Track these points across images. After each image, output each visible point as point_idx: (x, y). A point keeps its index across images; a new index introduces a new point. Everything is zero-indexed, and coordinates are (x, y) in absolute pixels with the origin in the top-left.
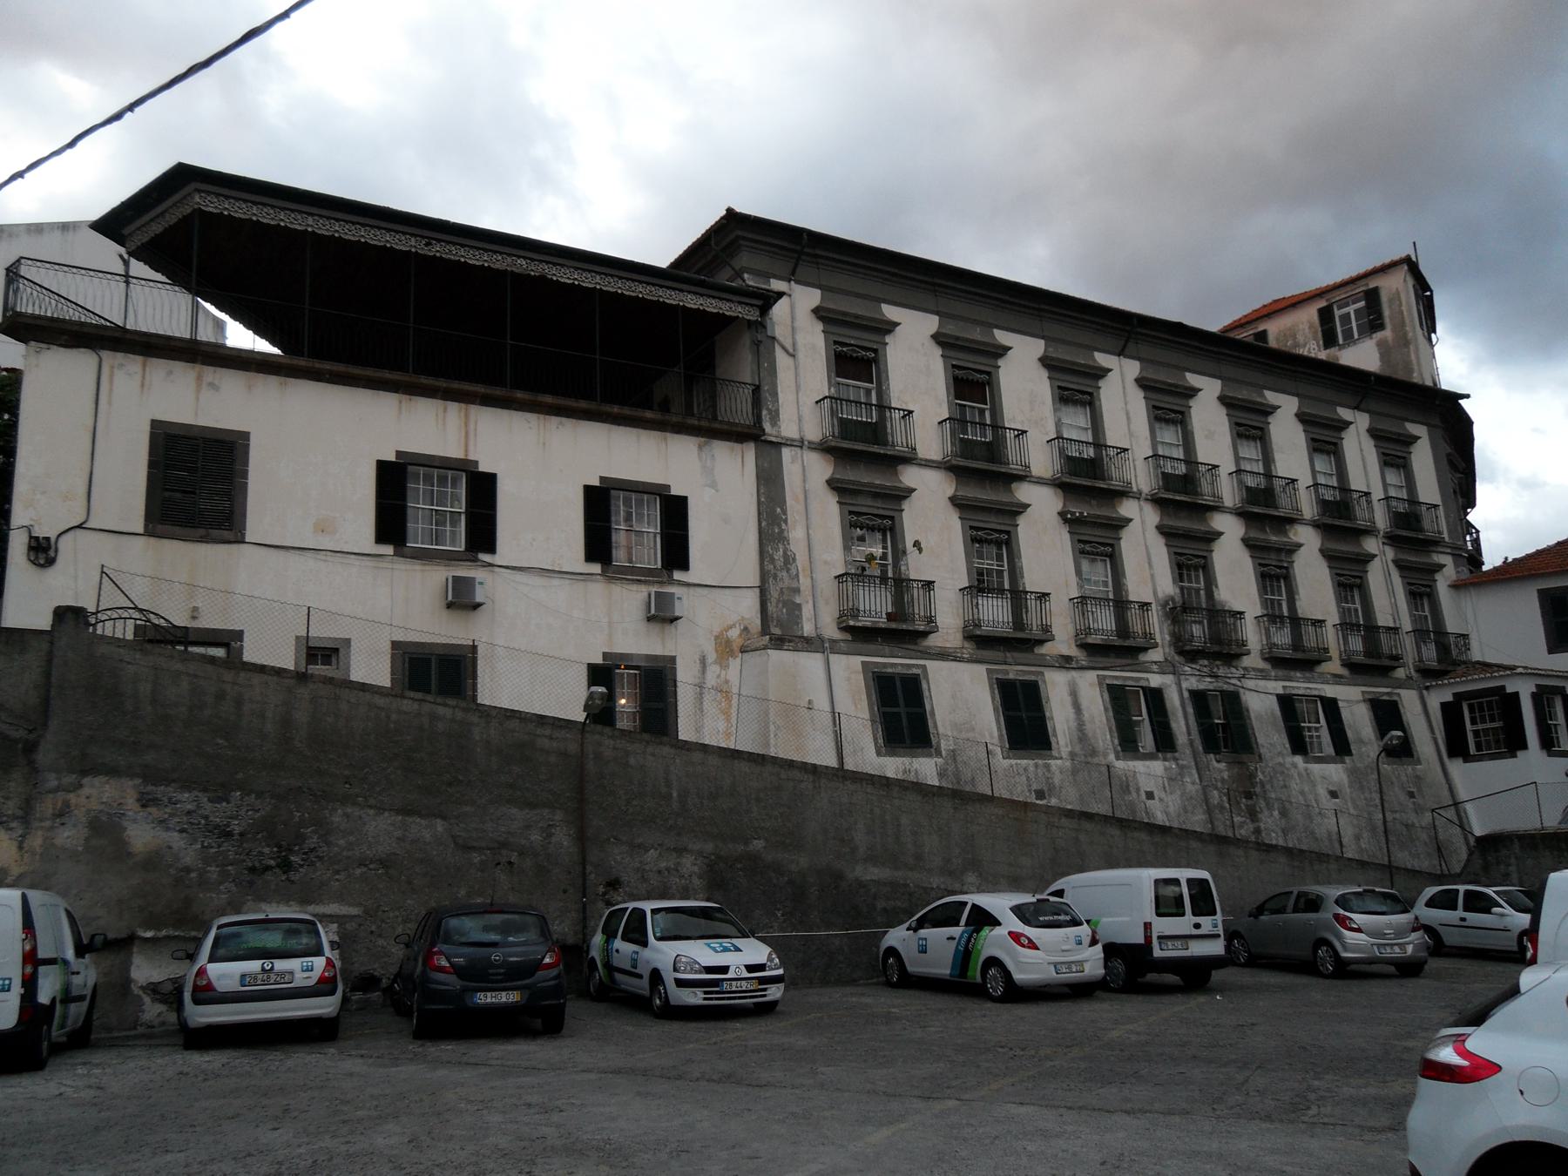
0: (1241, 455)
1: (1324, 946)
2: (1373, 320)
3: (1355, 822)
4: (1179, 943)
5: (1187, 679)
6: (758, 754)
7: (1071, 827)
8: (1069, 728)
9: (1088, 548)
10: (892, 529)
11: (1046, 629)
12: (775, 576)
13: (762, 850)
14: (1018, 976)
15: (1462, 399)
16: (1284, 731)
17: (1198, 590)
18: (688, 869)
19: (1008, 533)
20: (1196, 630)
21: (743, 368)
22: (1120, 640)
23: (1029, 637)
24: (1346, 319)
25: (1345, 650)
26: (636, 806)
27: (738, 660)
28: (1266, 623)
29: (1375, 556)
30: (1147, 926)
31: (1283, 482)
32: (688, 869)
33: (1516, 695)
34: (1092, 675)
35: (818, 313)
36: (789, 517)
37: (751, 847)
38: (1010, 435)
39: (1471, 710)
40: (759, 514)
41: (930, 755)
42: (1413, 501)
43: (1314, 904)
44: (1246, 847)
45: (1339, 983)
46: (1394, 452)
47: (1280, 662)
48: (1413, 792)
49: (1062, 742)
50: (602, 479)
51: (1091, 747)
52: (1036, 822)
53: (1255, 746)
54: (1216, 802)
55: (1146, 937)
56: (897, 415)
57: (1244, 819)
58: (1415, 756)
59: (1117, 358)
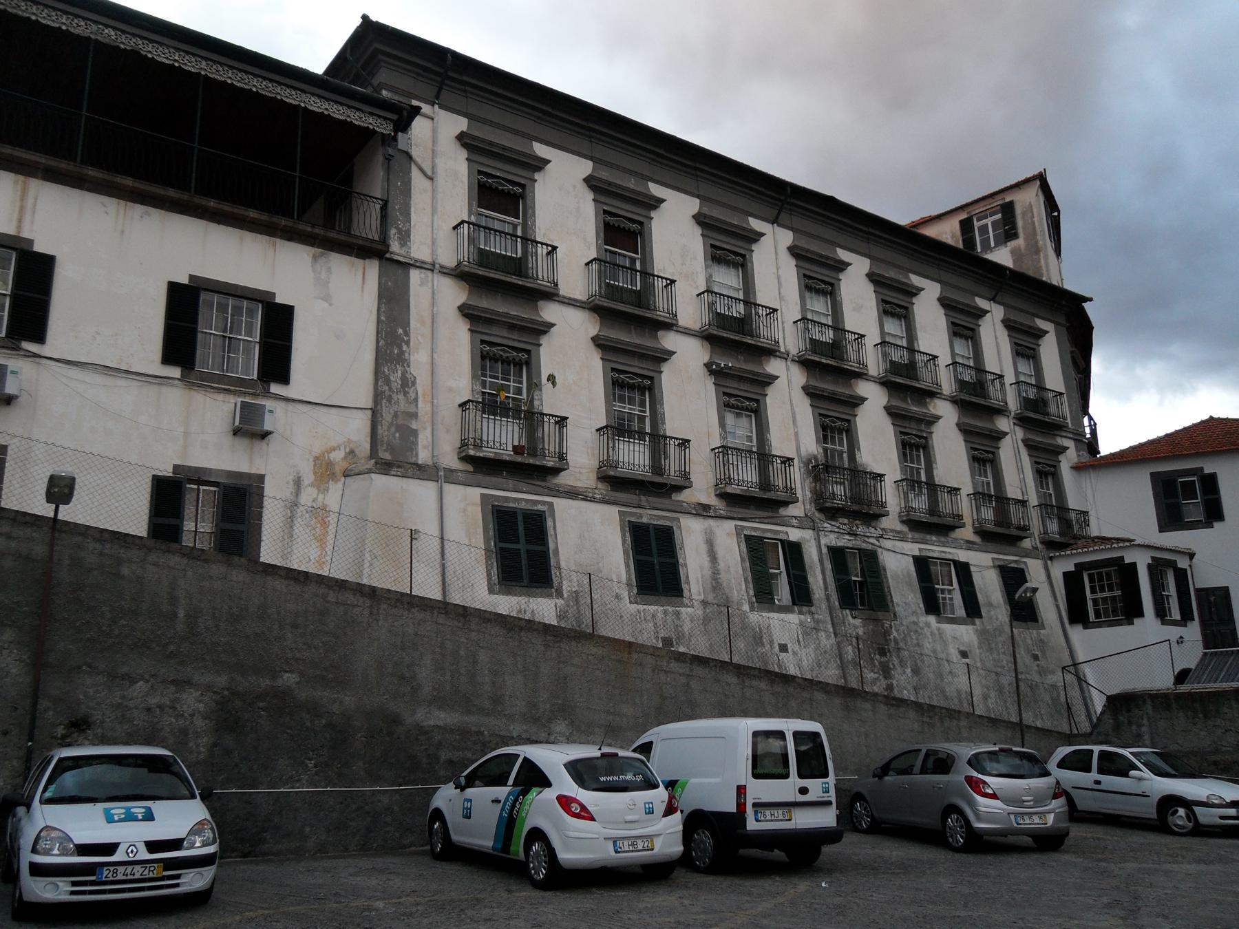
0: (886, 331)
1: (954, 813)
2: (1008, 231)
3: (984, 682)
4: (780, 812)
5: (826, 536)
6: (300, 572)
7: (681, 671)
8: (702, 576)
9: (733, 401)
10: (528, 363)
11: (686, 476)
12: (389, 399)
13: (294, 685)
14: (566, 856)
15: (1086, 302)
16: (919, 591)
17: (841, 453)
18: (189, 707)
19: (651, 378)
20: (839, 490)
21: (375, 183)
22: (762, 493)
23: (665, 481)
24: (984, 229)
25: (978, 519)
26: (123, 626)
27: (340, 485)
28: (905, 488)
29: (1007, 434)
30: (741, 790)
31: (926, 358)
32: (189, 707)
33: (1133, 566)
34: (730, 525)
35: (462, 138)
36: (412, 339)
37: (279, 682)
38: (659, 284)
39: (1091, 580)
40: (378, 332)
41: (550, 596)
42: (1041, 387)
43: (943, 764)
44: (874, 701)
45: (970, 858)
46: (1026, 348)
47: (917, 526)
48: (1037, 655)
49: (694, 590)
50: (192, 277)
51: (724, 597)
52: (641, 665)
53: (890, 604)
54: (850, 657)
55: (738, 805)
56: (542, 251)
57: (876, 675)
58: (1040, 621)
59: (771, 225)
